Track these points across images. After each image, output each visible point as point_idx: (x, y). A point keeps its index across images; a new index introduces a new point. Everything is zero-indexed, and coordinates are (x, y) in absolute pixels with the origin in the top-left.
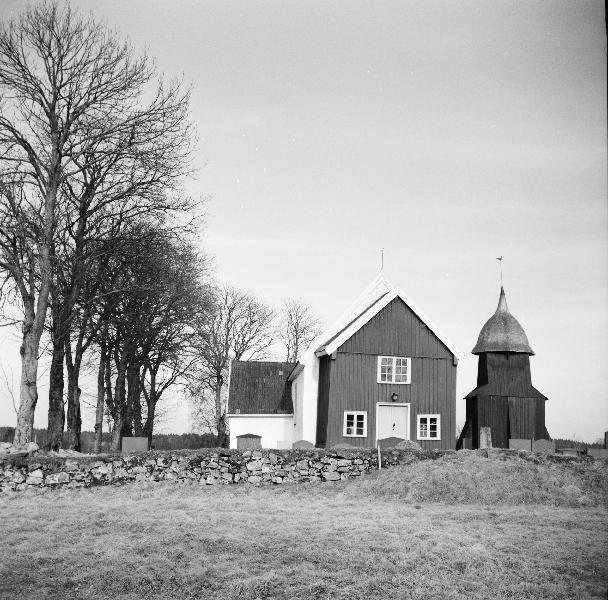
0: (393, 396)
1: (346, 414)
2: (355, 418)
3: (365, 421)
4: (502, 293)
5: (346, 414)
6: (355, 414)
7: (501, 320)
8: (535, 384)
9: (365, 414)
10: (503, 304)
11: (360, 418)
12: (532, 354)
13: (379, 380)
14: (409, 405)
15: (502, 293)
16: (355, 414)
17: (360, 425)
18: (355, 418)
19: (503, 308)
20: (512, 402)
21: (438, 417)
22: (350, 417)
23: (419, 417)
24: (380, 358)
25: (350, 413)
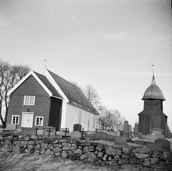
0: (28, 110)
1: (13, 116)
2: (16, 117)
3: (19, 119)
4: (154, 77)
5: (43, 118)
6: (16, 116)
7: (153, 87)
8: (143, 110)
9: (19, 116)
10: (154, 81)
11: (17, 117)
12: (164, 100)
13: (24, 104)
14: (33, 113)
15: (154, 77)
16: (16, 116)
17: (17, 120)
18: (16, 117)
19: (153, 83)
20: (152, 117)
21: (43, 118)
22: (14, 117)
23: (37, 117)
24: (25, 96)
25: (14, 116)
